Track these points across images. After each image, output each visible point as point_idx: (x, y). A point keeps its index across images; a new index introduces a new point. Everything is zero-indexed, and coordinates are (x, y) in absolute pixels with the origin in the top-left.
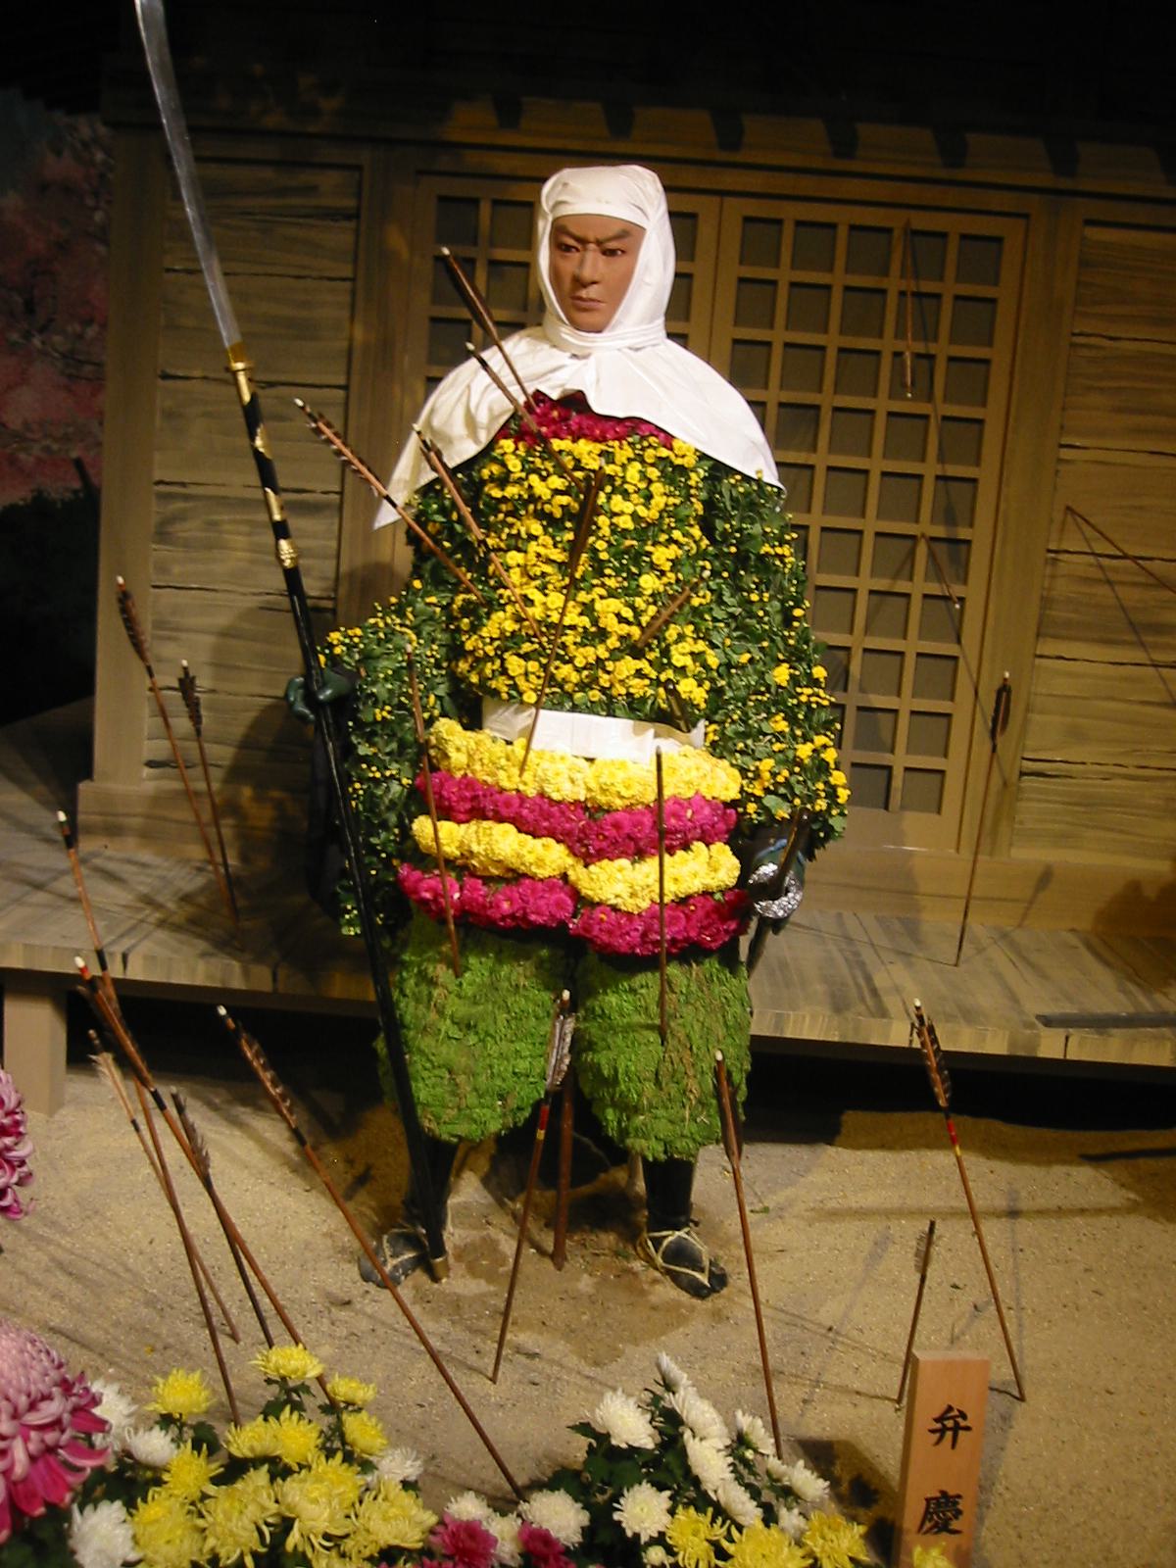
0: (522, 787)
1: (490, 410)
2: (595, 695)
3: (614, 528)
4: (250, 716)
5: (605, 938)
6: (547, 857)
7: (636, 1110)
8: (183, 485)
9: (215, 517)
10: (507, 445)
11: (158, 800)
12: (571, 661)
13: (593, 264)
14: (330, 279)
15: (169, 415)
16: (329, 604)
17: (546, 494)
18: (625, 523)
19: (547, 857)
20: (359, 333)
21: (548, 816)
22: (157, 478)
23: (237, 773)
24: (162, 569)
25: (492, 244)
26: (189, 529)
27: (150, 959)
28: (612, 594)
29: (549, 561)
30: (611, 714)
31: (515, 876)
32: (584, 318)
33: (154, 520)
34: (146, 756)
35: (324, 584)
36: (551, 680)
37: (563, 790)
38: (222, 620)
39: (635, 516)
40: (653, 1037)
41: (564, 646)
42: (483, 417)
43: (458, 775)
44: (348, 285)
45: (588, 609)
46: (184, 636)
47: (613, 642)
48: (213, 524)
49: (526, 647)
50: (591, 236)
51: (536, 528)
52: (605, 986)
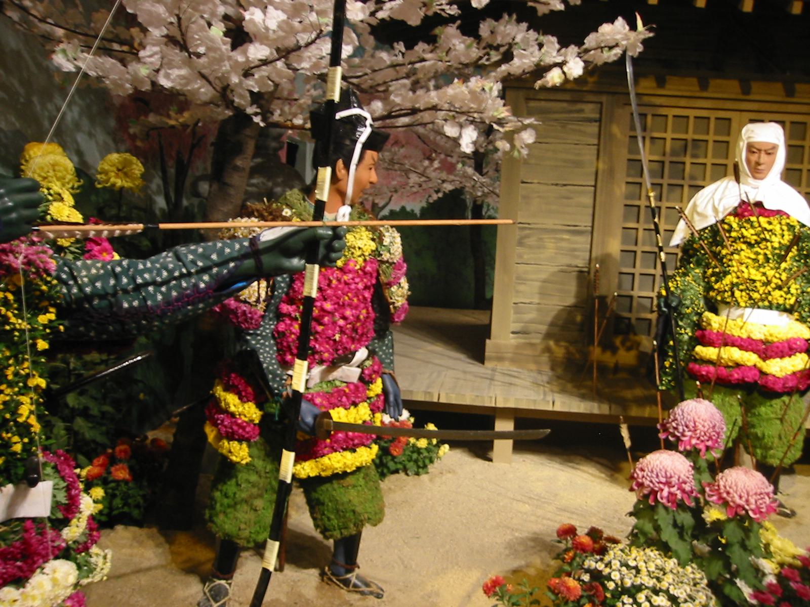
0: (741, 335)
1: (724, 207)
2: (766, 303)
3: (772, 247)
4: (553, 313)
5: (772, 386)
6: (750, 358)
7: (771, 448)
8: (529, 224)
9: (541, 236)
10: (732, 218)
11: (518, 347)
12: (758, 292)
13: (764, 158)
14: (589, 145)
15: (524, 197)
16: (586, 269)
17: (749, 236)
18: (776, 245)
19: (750, 358)
20: (601, 166)
21: (751, 344)
22: (519, 221)
23: (548, 336)
24: (520, 256)
25: (652, 131)
26: (531, 241)
27: (563, 403)
28: (772, 269)
29: (749, 258)
30: (771, 309)
31: (738, 365)
32: (757, 175)
33: (518, 237)
34: (512, 330)
35: (584, 262)
36: (751, 298)
37: (757, 335)
38: (543, 276)
39: (780, 243)
40: (778, 422)
41: (756, 287)
42: (721, 209)
43: (715, 331)
44: (596, 147)
45: (764, 274)
46: (527, 282)
47: (773, 285)
48: (541, 239)
49: (741, 287)
50: (763, 148)
51: (744, 247)
52: (761, 404)
